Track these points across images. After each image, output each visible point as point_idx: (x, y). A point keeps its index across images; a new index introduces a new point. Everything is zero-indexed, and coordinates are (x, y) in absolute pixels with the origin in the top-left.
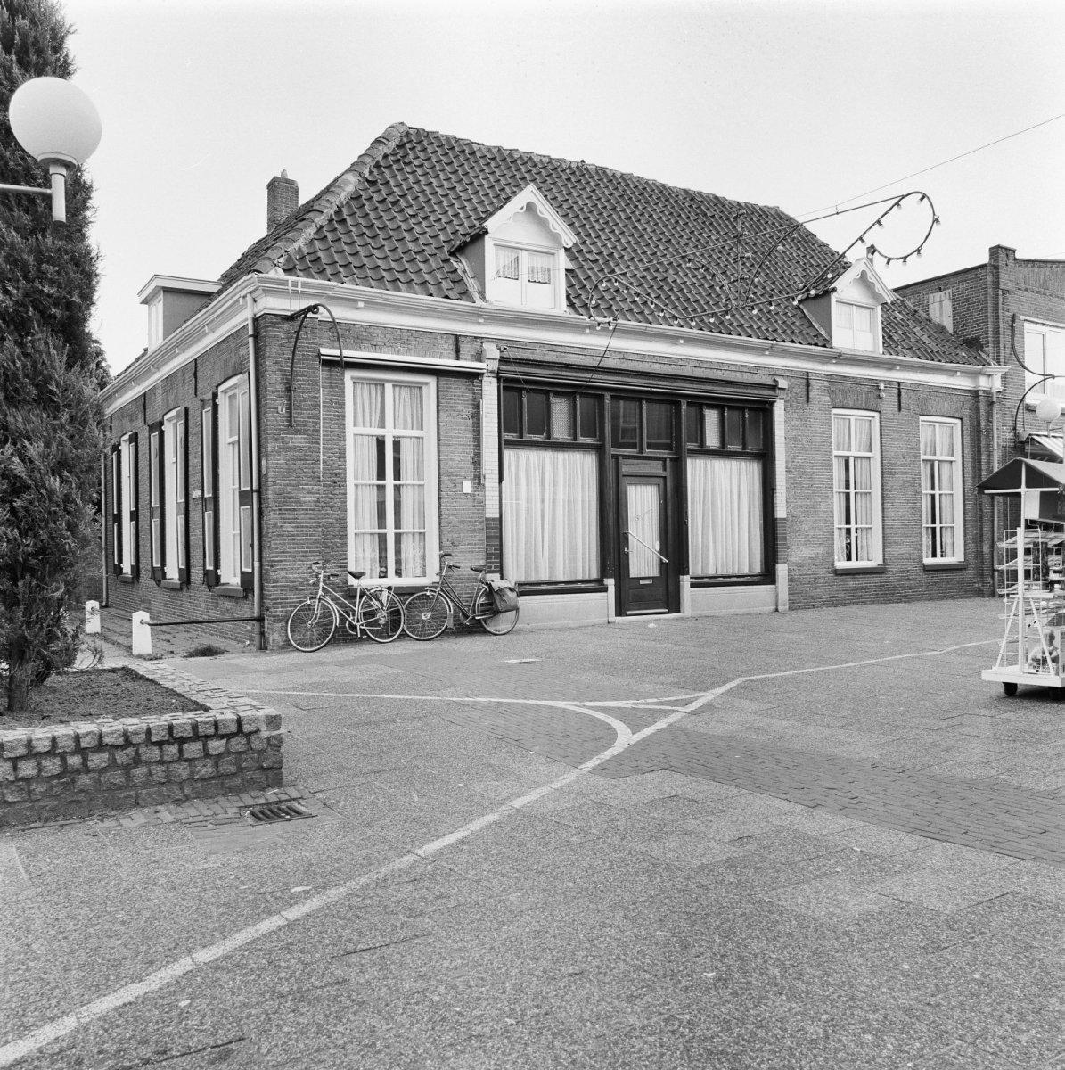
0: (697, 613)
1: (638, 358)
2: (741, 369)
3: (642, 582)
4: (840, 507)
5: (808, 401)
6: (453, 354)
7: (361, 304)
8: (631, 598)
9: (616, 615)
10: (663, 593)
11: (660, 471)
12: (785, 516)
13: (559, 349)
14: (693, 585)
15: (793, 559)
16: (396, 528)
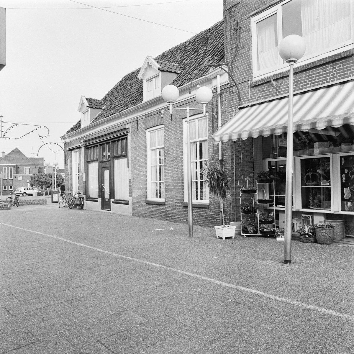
7: (105, 123)
14: (113, 202)
16: (160, 181)
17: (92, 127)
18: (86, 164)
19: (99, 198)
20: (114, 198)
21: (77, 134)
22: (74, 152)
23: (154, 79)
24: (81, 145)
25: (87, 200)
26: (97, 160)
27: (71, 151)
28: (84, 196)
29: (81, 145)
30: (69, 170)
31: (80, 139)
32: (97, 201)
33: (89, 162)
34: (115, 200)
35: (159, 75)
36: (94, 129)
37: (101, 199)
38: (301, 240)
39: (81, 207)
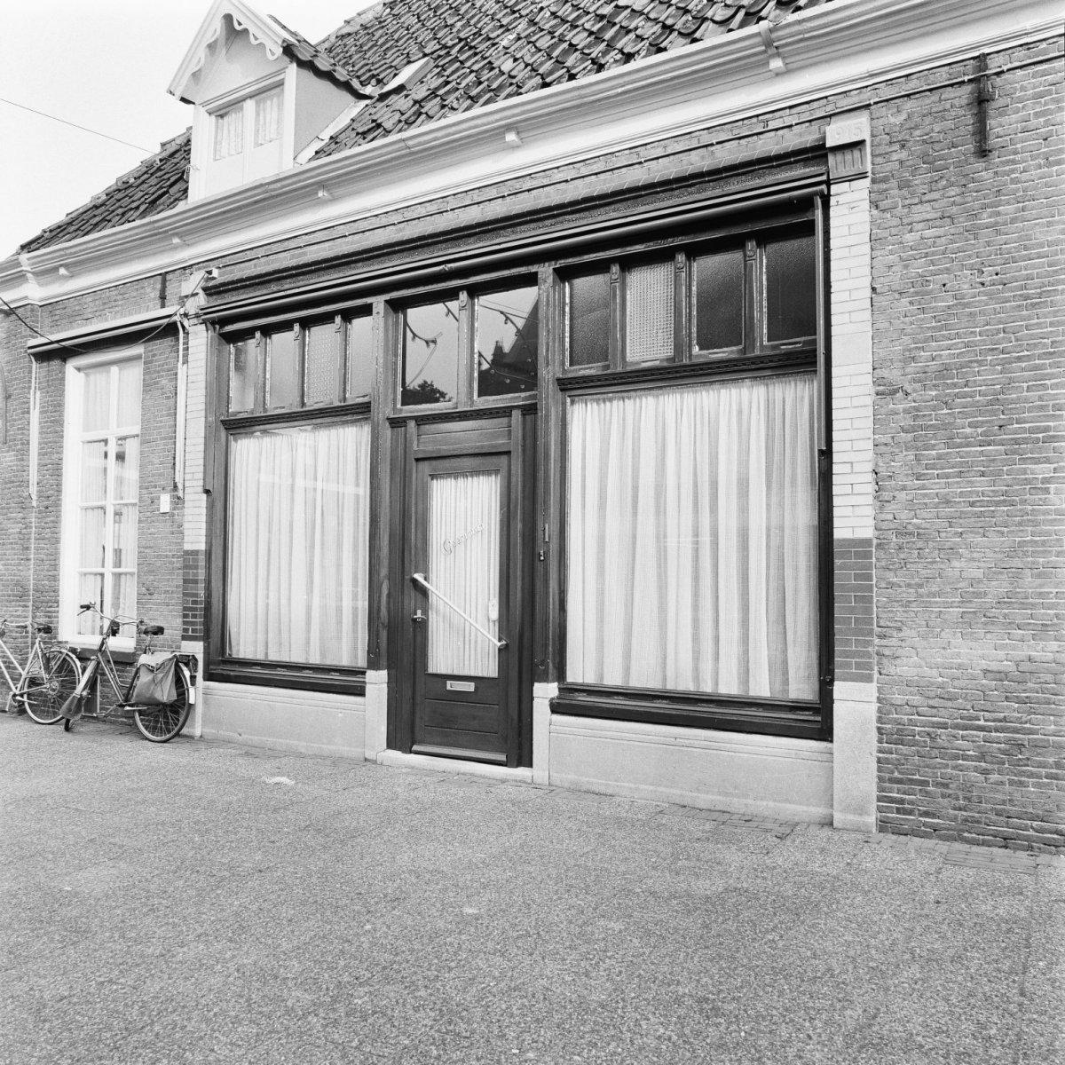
0: (565, 778)
1: (432, 208)
2: (706, 138)
3: (452, 686)
4: (357, 525)
5: (983, 153)
6: (158, 302)
7: (62, 271)
8: (429, 713)
9: (391, 744)
10: (492, 720)
11: (337, 463)
12: (868, 533)
13: (292, 244)
14: (556, 708)
15: (906, 668)
16: (115, 566)
17: (322, 185)
18: (217, 439)
19: (373, 664)
20: (561, 675)
21: (159, 238)
22: (79, 369)
23: (250, 105)
24: (182, 311)
25: (209, 677)
26: (358, 411)
27: (55, 364)
28: (196, 649)
29: (186, 315)
30: (33, 476)
31: (164, 282)
32: (359, 691)
33: (238, 426)
34: (567, 690)
35: (281, 84)
36: (334, 199)
37: (383, 674)
38: (328, 762)
39: (168, 718)
